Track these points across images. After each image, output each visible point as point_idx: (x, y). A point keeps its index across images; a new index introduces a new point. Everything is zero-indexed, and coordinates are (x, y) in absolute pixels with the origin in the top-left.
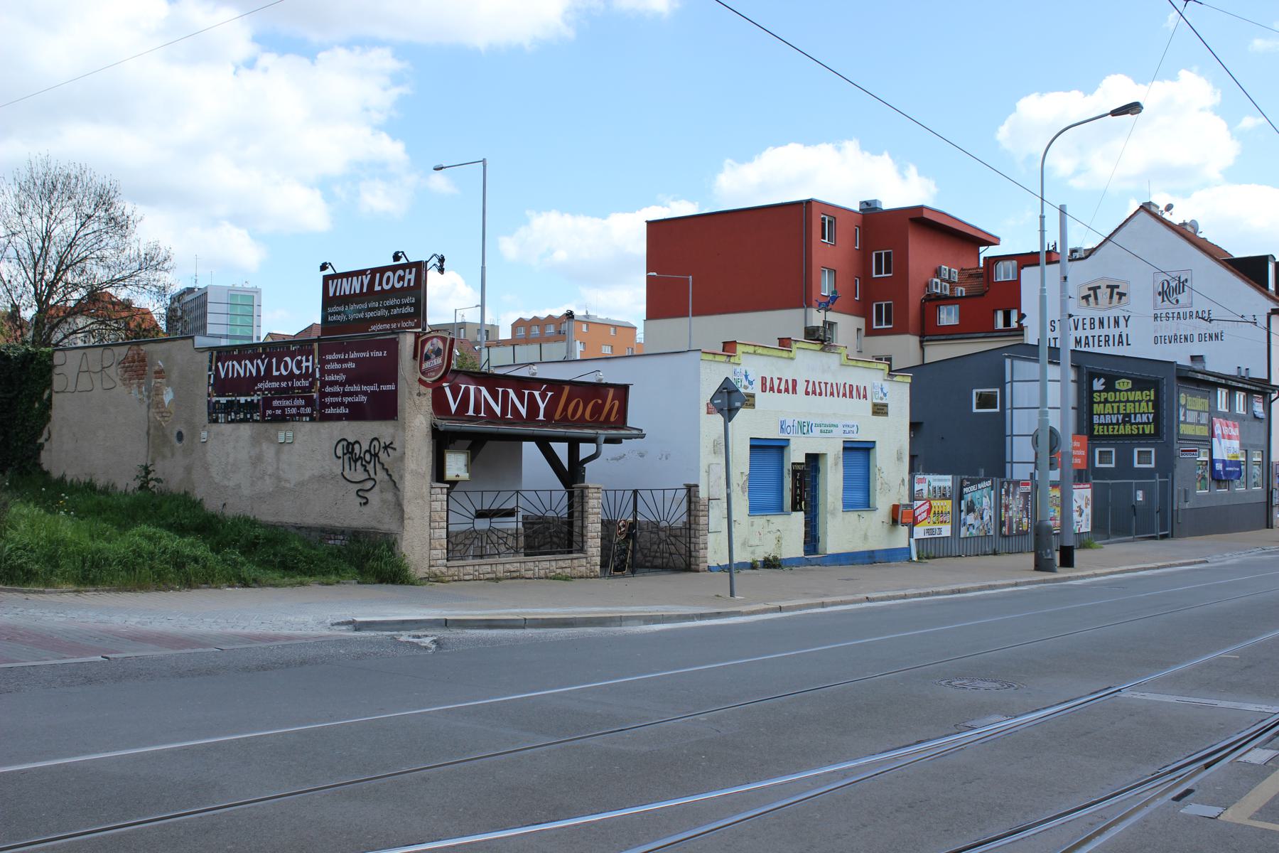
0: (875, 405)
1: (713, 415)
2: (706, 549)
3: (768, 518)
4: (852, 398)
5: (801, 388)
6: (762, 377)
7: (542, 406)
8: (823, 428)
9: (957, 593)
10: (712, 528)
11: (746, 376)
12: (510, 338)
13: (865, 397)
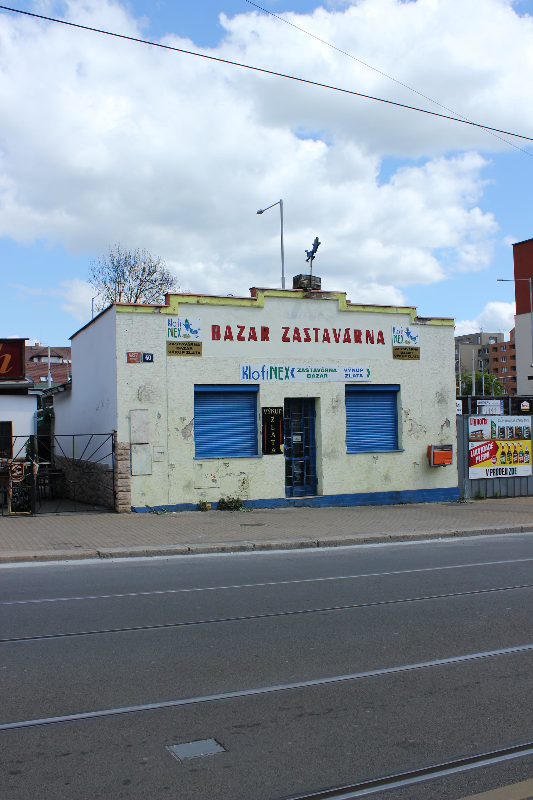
0: (396, 349)
1: (138, 364)
2: (128, 491)
3: (226, 461)
4: (360, 342)
5: (276, 334)
6: (213, 327)
7: (269, 412)
8: (312, 373)
9: (314, 547)
10: (136, 469)
11: (187, 326)
12: (510, 341)
13: (381, 340)
